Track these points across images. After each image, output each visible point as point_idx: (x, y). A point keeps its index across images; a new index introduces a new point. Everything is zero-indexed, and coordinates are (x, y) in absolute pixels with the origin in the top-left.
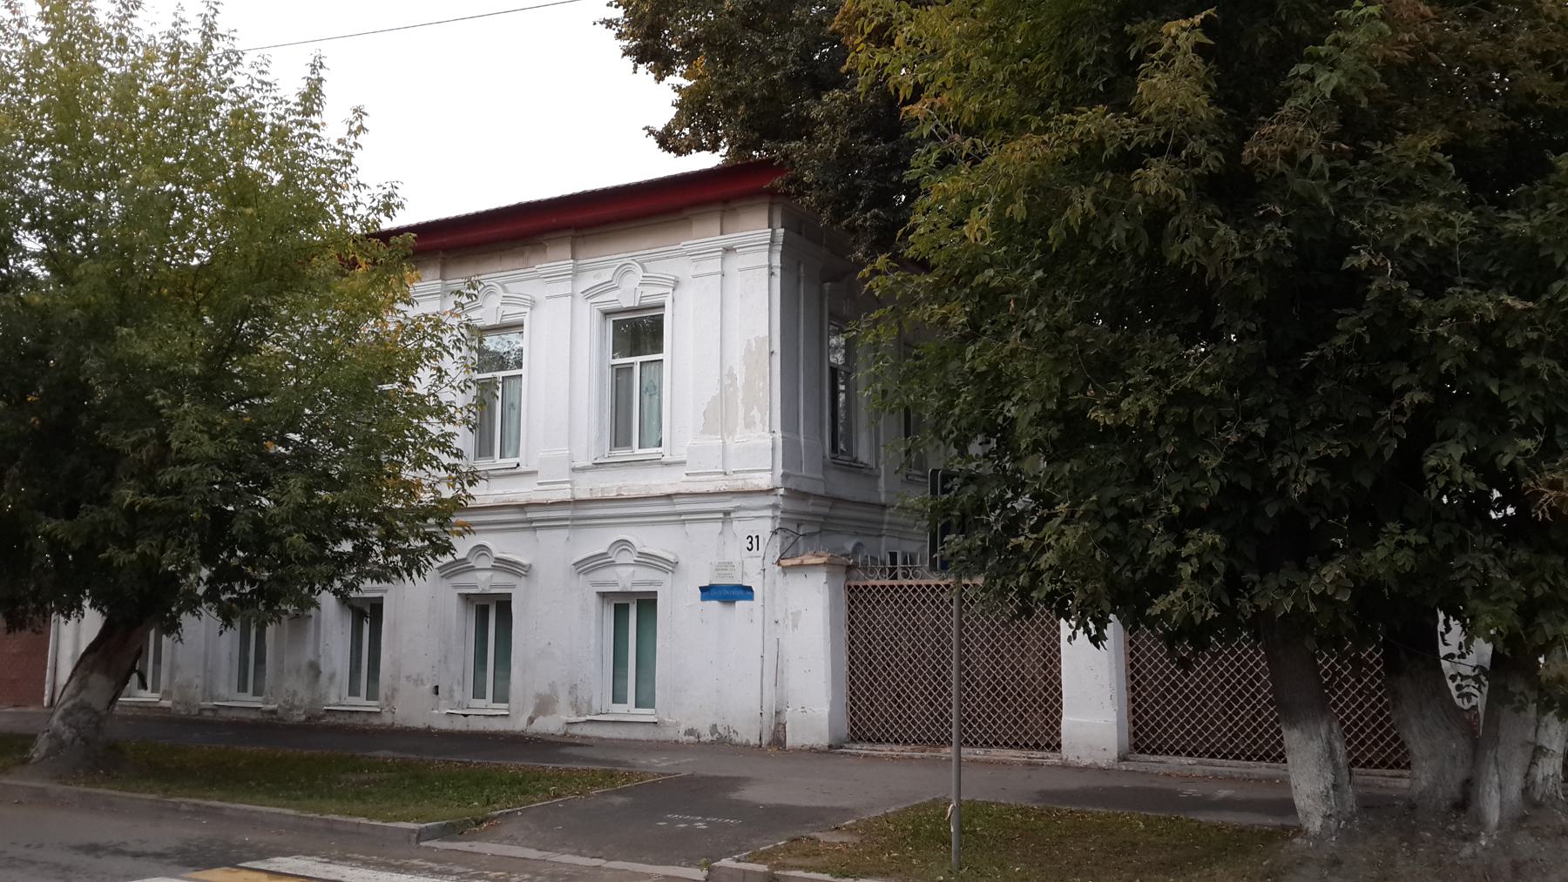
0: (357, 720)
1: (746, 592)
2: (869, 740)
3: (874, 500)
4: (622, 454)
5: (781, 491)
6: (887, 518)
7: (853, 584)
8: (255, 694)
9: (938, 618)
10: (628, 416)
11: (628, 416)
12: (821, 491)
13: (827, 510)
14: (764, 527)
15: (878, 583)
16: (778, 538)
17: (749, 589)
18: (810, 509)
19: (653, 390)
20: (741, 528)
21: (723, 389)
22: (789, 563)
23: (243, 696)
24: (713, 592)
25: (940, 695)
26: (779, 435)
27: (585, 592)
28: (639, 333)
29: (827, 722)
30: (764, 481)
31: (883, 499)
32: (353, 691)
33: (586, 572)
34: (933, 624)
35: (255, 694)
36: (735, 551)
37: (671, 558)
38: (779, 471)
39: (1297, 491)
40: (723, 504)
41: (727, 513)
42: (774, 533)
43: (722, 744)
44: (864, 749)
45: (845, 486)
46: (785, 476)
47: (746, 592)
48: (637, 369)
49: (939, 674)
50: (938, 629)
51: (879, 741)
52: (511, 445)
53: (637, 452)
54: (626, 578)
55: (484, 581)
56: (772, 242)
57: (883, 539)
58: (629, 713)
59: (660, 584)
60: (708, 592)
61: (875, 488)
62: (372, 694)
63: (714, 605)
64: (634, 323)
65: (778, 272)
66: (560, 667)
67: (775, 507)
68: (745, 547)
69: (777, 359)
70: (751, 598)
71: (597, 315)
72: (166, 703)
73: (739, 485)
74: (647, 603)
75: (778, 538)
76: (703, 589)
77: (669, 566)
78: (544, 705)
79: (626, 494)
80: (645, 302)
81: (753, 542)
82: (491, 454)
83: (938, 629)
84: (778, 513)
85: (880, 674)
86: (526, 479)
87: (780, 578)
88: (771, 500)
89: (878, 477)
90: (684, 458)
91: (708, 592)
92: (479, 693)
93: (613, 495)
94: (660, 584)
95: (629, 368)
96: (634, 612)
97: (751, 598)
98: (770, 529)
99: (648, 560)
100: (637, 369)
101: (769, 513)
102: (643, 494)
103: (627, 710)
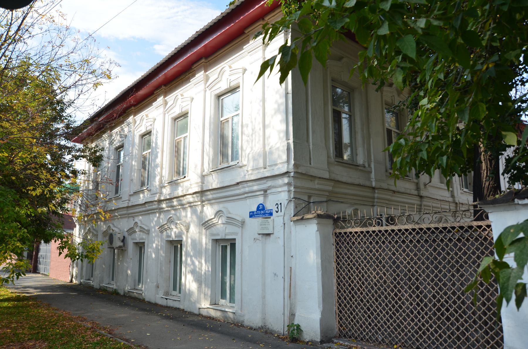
3: (367, 183)
5: (292, 174)
6: (376, 195)
7: (338, 231)
9: (394, 254)
12: (327, 176)
13: (330, 188)
15: (353, 230)
16: (292, 205)
18: (317, 187)
25: (397, 311)
29: (319, 326)
31: (374, 184)
34: (390, 258)
38: (292, 162)
41: (265, 191)
45: (343, 174)
46: (295, 165)
49: (396, 295)
50: (394, 263)
57: (375, 208)
61: (369, 179)
69: (290, 96)
83: (394, 263)
84: (292, 188)
85: (356, 293)
87: (293, 228)
88: (286, 180)
89: (371, 172)
94: (236, 234)
98: (287, 198)
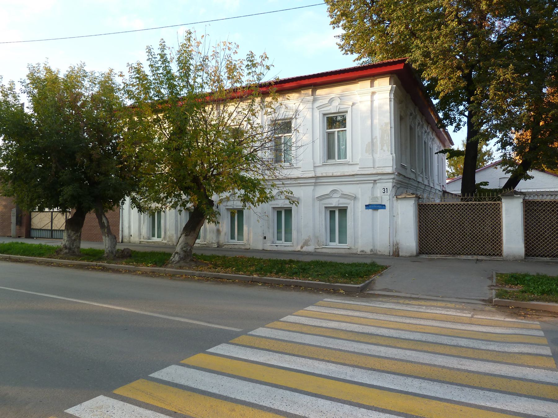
0: (236, 247)
1: (383, 207)
2: (427, 253)
4: (331, 161)
8: (286, 241)
10: (332, 150)
11: (332, 150)
14: (389, 185)
16: (394, 189)
17: (385, 205)
19: (342, 141)
20: (379, 186)
21: (372, 139)
22: (397, 196)
23: (233, 241)
24: (370, 207)
26: (394, 155)
27: (319, 207)
28: (335, 121)
30: (390, 170)
32: (233, 237)
33: (320, 200)
35: (286, 241)
36: (378, 192)
37: (354, 195)
39: (243, 192)
40: (374, 178)
41: (375, 181)
42: (393, 187)
43: (374, 254)
44: (424, 256)
47: (383, 207)
48: (336, 133)
51: (430, 253)
52: (343, 154)
53: (337, 161)
54: (334, 202)
55: (282, 203)
56: (391, 90)
58: (336, 245)
59: (349, 204)
60: (368, 207)
62: (343, 240)
63: (370, 211)
64: (332, 118)
65: (393, 100)
66: (309, 232)
67: (394, 179)
68: (383, 191)
69: (393, 129)
70: (385, 208)
71: (321, 115)
72: (165, 242)
73: (380, 171)
74: (343, 211)
75: (394, 189)
76: (366, 206)
77: (355, 198)
78: (306, 243)
79: (335, 174)
80: (341, 110)
81: (385, 190)
82: (334, 158)
84: (395, 181)
86: (356, 166)
88: (392, 176)
90: (358, 163)
91: (368, 207)
92: (279, 239)
93: (331, 175)
94: (349, 204)
95: (333, 133)
96: (338, 215)
97: (385, 208)
99: (344, 196)
100: (336, 133)
101: (391, 181)
102: (342, 174)
103: (336, 244)
